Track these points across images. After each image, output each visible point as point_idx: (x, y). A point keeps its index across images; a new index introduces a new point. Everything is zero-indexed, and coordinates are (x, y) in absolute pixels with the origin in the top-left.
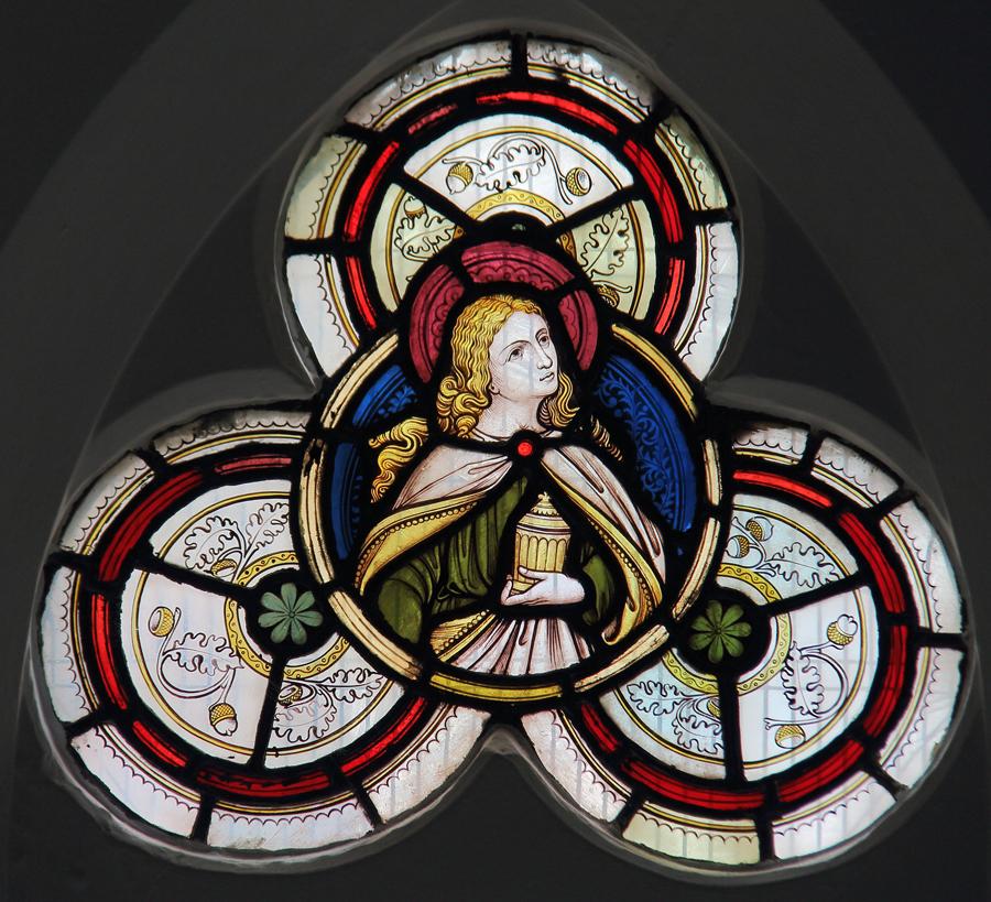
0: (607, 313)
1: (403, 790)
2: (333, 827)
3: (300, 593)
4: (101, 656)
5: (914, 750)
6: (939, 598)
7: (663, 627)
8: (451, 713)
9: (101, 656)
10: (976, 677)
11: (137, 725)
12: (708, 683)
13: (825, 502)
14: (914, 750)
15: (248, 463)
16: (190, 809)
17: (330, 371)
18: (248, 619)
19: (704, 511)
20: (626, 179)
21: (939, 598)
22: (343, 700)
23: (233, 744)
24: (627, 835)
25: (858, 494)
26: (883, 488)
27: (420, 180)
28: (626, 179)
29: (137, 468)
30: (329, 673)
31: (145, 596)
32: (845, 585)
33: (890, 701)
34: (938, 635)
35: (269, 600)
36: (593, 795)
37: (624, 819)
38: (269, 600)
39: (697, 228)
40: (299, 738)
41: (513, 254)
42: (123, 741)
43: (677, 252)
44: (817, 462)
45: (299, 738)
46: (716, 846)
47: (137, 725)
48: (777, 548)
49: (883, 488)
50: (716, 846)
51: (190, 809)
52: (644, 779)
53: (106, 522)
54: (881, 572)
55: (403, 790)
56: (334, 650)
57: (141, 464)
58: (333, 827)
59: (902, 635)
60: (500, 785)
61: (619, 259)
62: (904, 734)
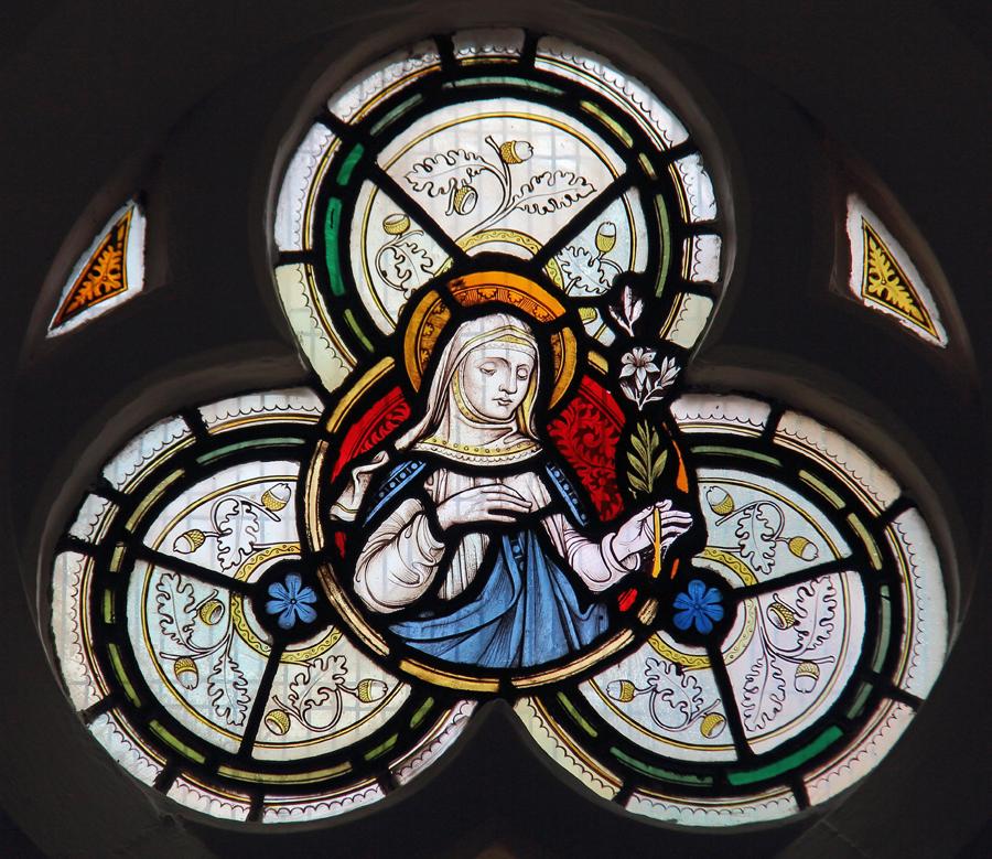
2: (81, 682)
7: (392, 331)
10: (36, 613)
11: (851, 714)
15: (348, 612)
17: (527, 661)
18: (255, 610)
19: (387, 444)
24: (813, 802)
26: (270, 817)
27: (732, 742)
34: (903, 692)
35: (307, 615)
38: (307, 615)
42: (88, 611)
44: (695, 239)
47: (851, 714)
49: (270, 817)
56: (233, 608)
62: (876, 726)
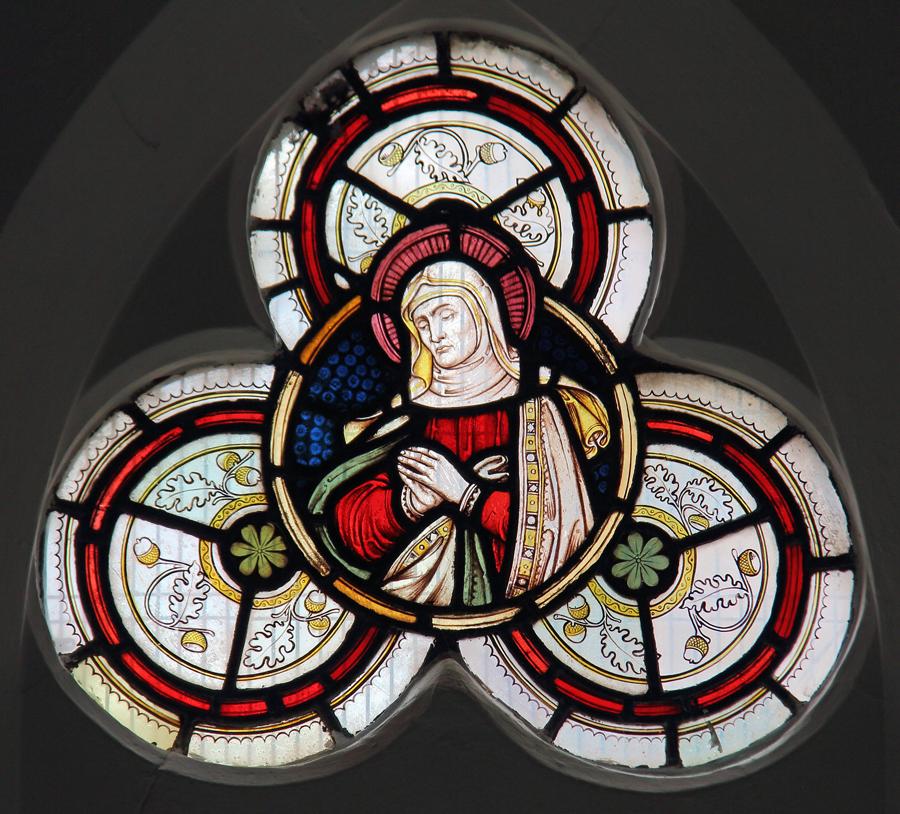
0: (544, 286)
1: (362, 709)
2: (298, 743)
3: (241, 540)
4: (97, 596)
5: (810, 669)
6: (830, 523)
8: (401, 637)
9: (97, 596)
12: (684, 562)
13: (708, 437)
14: (810, 669)
16: (170, 732)
20: (545, 163)
21: (830, 523)
22: (297, 632)
23: (206, 666)
25: (597, 163)
28: (545, 163)
29: (124, 421)
30: (664, 506)
31: (131, 535)
32: (749, 521)
33: (788, 616)
36: (531, 708)
37: (553, 727)
39: (563, 122)
40: (724, 494)
41: (452, 226)
43: (594, 221)
45: (724, 494)
46: (635, 750)
48: (681, 487)
50: (635, 750)
51: (170, 732)
52: (575, 695)
53: (53, 475)
54: (777, 507)
55: (362, 709)
57: (128, 419)
58: (298, 743)
59: (800, 565)
60: (447, 701)
61: (546, 232)
